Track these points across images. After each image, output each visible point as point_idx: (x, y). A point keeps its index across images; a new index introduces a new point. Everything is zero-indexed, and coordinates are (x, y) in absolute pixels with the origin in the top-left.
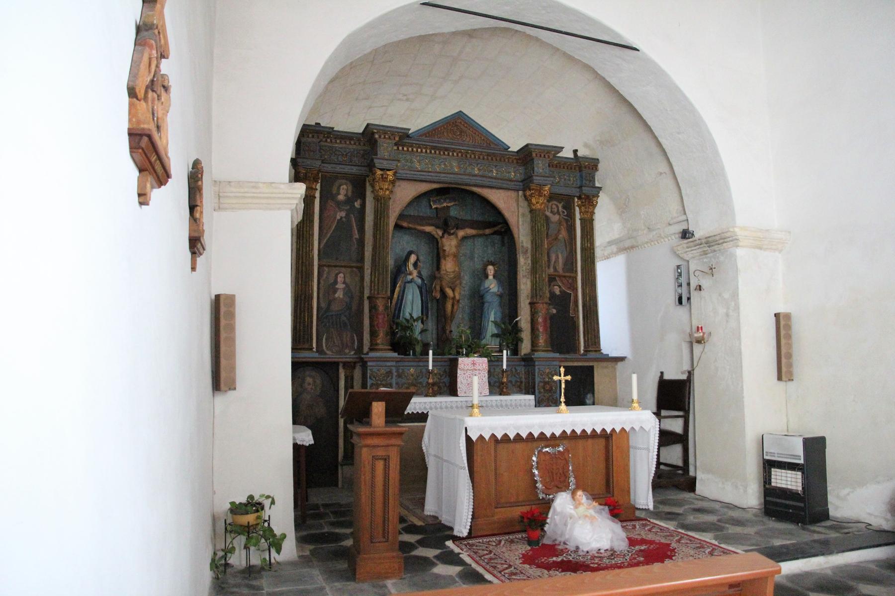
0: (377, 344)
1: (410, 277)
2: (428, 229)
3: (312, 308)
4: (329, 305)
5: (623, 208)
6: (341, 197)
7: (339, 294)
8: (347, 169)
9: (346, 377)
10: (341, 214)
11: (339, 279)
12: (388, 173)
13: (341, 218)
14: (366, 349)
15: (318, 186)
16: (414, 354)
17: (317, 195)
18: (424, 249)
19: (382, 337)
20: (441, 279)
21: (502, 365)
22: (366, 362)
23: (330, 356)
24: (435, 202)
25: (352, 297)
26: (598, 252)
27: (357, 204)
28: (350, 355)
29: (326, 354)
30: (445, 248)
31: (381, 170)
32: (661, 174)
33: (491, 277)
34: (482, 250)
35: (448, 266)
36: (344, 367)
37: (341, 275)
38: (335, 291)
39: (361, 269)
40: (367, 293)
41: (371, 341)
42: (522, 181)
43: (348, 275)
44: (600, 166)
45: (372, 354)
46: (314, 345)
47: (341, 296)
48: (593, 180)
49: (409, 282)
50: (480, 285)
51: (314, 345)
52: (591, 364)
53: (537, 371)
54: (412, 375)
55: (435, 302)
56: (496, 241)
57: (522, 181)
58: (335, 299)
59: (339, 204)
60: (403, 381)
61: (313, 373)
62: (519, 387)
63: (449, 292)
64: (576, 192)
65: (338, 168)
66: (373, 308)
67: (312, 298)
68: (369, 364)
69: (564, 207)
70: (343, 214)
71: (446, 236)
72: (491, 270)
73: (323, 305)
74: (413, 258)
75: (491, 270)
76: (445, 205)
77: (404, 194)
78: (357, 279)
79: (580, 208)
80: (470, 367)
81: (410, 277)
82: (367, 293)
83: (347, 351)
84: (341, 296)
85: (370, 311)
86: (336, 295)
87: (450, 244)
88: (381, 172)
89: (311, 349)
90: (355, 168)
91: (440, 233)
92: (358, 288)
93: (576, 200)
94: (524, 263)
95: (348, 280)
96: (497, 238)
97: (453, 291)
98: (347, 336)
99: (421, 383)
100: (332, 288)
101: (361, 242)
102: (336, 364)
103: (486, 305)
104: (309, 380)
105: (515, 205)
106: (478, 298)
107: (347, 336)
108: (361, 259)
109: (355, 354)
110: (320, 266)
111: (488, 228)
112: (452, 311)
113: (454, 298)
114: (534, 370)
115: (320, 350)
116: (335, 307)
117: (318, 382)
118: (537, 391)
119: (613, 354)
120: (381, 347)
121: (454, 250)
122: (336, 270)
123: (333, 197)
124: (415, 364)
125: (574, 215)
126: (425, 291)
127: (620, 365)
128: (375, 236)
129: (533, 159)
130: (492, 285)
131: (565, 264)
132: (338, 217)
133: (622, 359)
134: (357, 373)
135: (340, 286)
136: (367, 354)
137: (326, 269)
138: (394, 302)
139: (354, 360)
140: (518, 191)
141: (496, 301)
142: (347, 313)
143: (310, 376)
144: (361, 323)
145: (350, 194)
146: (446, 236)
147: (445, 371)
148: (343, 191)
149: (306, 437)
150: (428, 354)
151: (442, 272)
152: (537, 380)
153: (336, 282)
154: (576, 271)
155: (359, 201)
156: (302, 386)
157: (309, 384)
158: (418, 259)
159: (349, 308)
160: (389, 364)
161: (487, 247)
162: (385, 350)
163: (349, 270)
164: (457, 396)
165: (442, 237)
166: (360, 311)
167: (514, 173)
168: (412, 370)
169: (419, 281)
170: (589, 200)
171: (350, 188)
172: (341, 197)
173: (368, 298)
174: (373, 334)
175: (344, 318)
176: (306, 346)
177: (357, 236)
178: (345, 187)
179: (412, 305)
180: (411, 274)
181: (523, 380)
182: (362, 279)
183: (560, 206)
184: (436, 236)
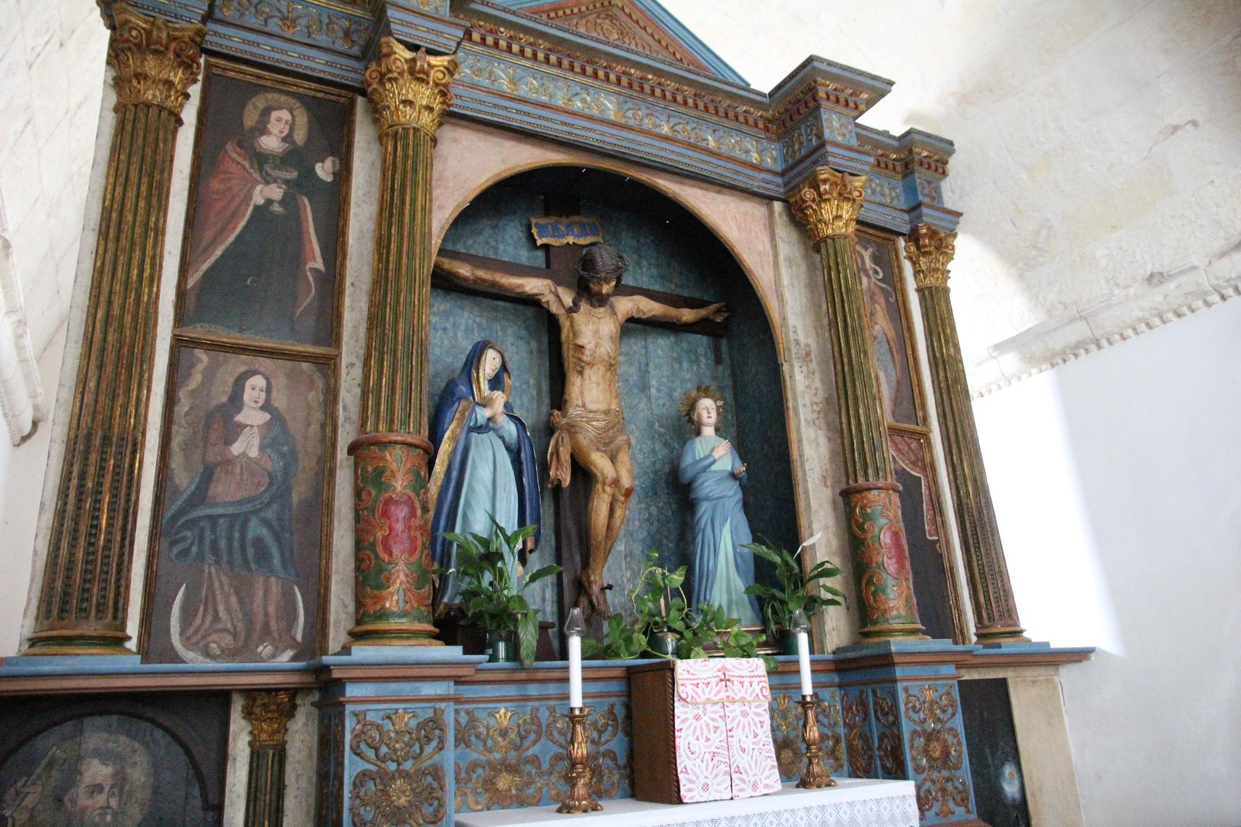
0: (382, 615)
1: (487, 413)
2: (533, 286)
3: (133, 484)
4: (208, 476)
5: (1024, 259)
6: (271, 143)
7: (247, 446)
8: (294, 57)
9: (256, 756)
10: (267, 193)
11: (248, 395)
12: (434, 60)
13: (269, 202)
14: (337, 636)
15: (195, 90)
16: (514, 654)
17: (189, 115)
18: (507, 351)
19: (398, 594)
20: (572, 429)
21: (799, 686)
22: (340, 683)
23: (196, 665)
24: (542, 229)
25: (291, 459)
26: (975, 377)
27: (324, 170)
28: (278, 662)
29: (178, 659)
30: (582, 341)
31: (414, 48)
32: (1176, 128)
33: (708, 431)
34: (672, 369)
35: (590, 394)
36: (248, 714)
37: (258, 381)
38: (233, 432)
39: (328, 365)
40: (346, 436)
41: (359, 604)
42: (782, 174)
43: (280, 382)
44: (953, 164)
45: (363, 652)
46: (133, 628)
47: (254, 453)
48: (936, 195)
49: (479, 429)
50: (679, 457)
51: (133, 628)
52: (1000, 674)
53: (902, 696)
54: (504, 733)
55: (560, 498)
56: (701, 350)
57: (782, 174)
58: (228, 462)
59: (261, 159)
60: (474, 756)
61: (122, 742)
62: (833, 753)
63: (600, 462)
64: (901, 223)
65: (267, 50)
66: (369, 481)
67: (138, 446)
68: (352, 691)
69: (876, 259)
70: (276, 192)
71: (584, 306)
72: (708, 410)
73: (183, 479)
74: (490, 363)
75: (708, 410)
76: (571, 240)
77: (469, 165)
78: (315, 397)
79: (914, 263)
80: (714, 692)
81: (487, 413)
82: (346, 436)
83: (265, 649)
84: (254, 453)
85: (358, 493)
86: (236, 449)
87: (594, 331)
88: (409, 55)
89: (117, 641)
90: (322, 57)
91: (568, 300)
92: (314, 428)
93: (901, 243)
94: (805, 388)
95: (280, 401)
96: (701, 342)
97: (613, 459)
98: (267, 592)
99: (535, 761)
100: (222, 421)
101: (332, 282)
102: (219, 699)
103: (704, 509)
104: (97, 771)
105: (764, 237)
106: (678, 493)
107: (267, 592)
108: (330, 330)
109: (294, 659)
110: (179, 344)
111: (692, 307)
112: (609, 527)
113: (616, 482)
114: (894, 696)
115: (154, 643)
116: (226, 491)
117: (139, 774)
118: (910, 766)
119: (1058, 642)
120: (394, 624)
121: (606, 348)
122: (239, 364)
123: (247, 141)
124: (510, 691)
125: (902, 279)
126: (530, 458)
127: (1067, 675)
128: (382, 245)
129: (818, 107)
130: (715, 454)
131: (896, 402)
132: (258, 199)
133: (1078, 656)
134: (301, 735)
135: (252, 416)
136: (346, 650)
137: (203, 356)
138: (434, 487)
139: (294, 679)
140: (771, 199)
141: (732, 494)
142: (270, 514)
143: (104, 756)
144: (323, 545)
145: (300, 136)
146: (584, 306)
147: (611, 712)
148: (281, 127)
149: (720, 403)
150: (564, 655)
151: (574, 411)
152: (906, 728)
153: (236, 399)
154: (925, 419)
155: (329, 163)
156: (59, 800)
157: (97, 788)
158: (504, 367)
159: (280, 489)
160: (428, 689)
161: (679, 360)
162: (415, 634)
163: (289, 364)
164: (679, 801)
165: (574, 309)
166: (321, 505)
167: (761, 154)
168: (503, 714)
169: (511, 429)
170: (932, 242)
171: (302, 119)
172: (271, 143)
173: (353, 449)
174: (368, 577)
175: (255, 529)
176: (92, 627)
177: (319, 264)
178: (285, 115)
179: (491, 499)
180: (485, 404)
181: (842, 731)
182: (331, 396)
183: (867, 255)
184: (554, 308)
